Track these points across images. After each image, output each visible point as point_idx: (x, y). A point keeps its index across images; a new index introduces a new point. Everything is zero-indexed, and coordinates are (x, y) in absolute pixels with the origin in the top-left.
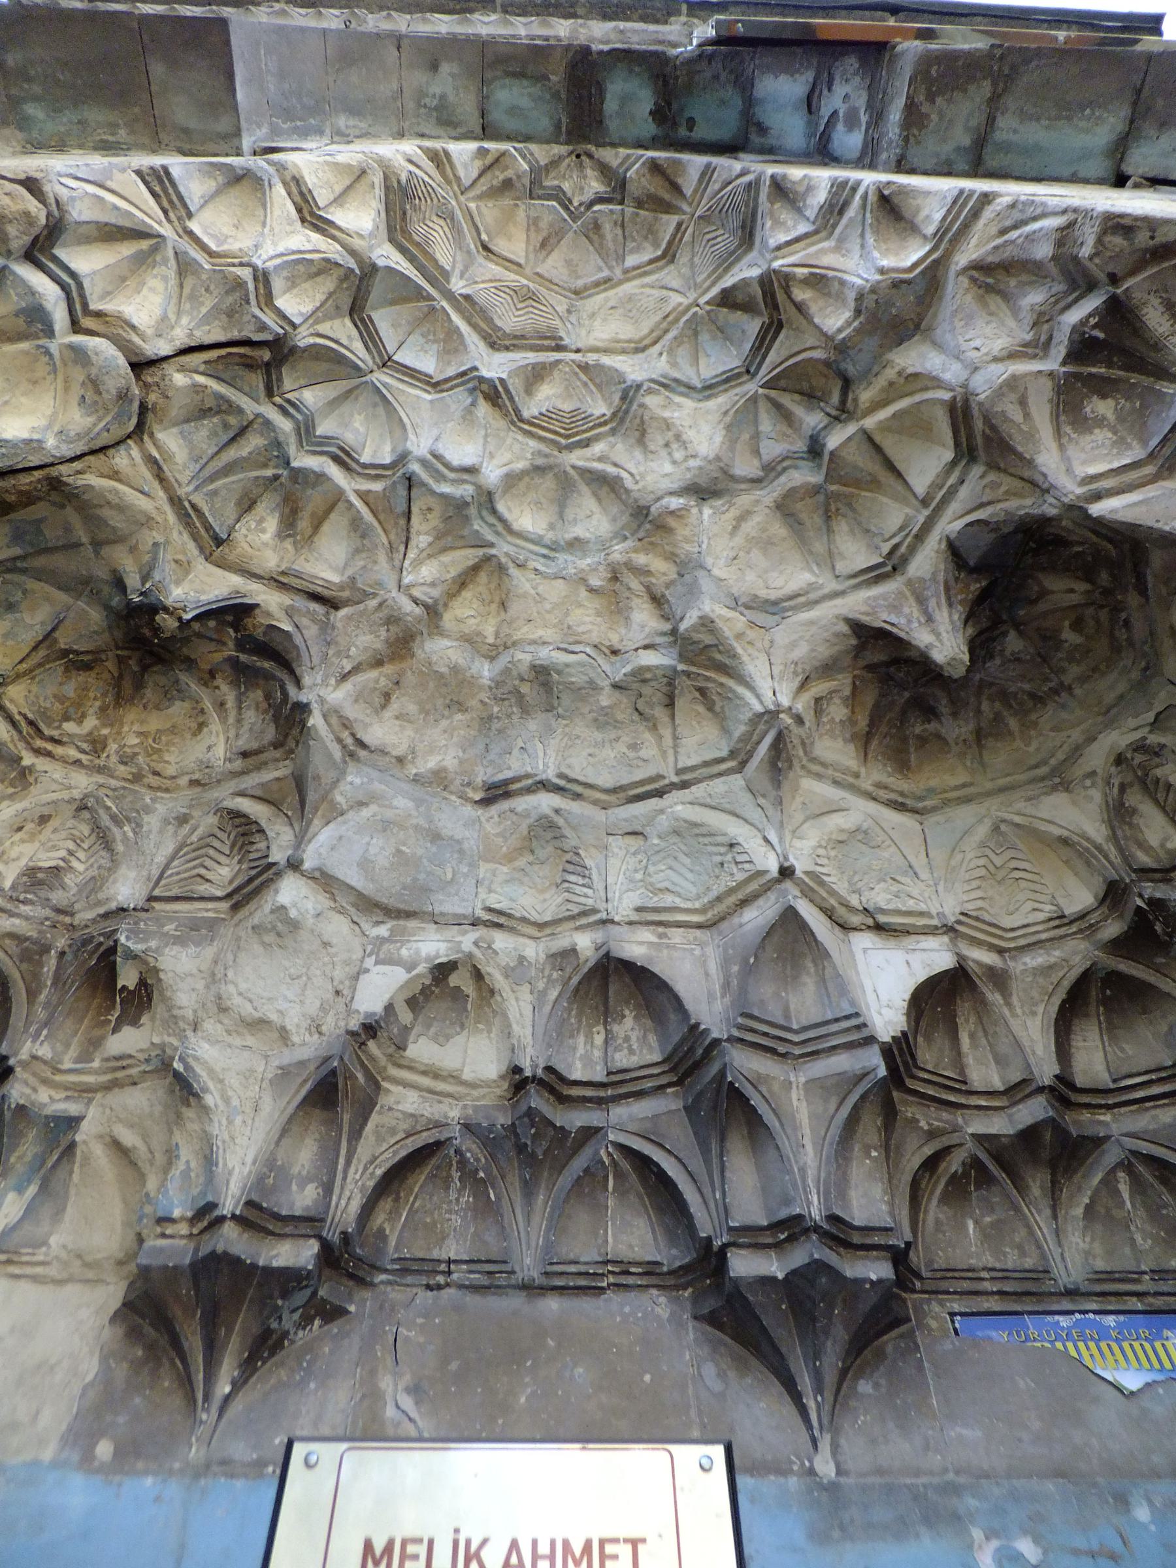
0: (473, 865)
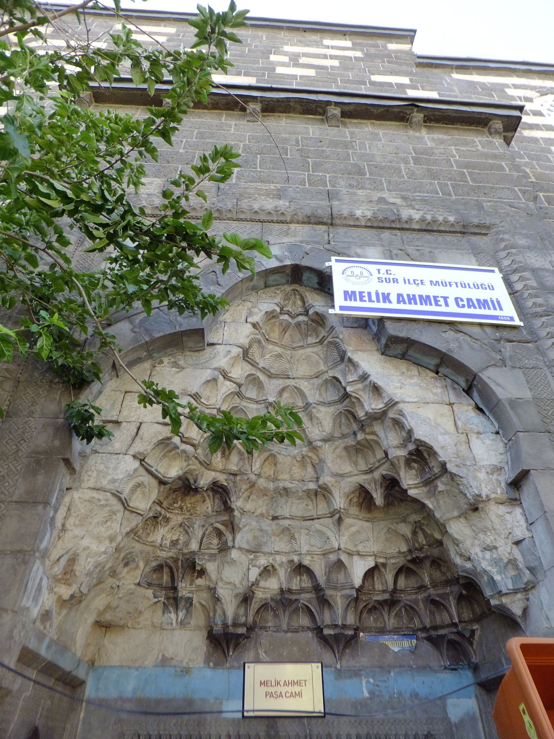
0: (270, 537)
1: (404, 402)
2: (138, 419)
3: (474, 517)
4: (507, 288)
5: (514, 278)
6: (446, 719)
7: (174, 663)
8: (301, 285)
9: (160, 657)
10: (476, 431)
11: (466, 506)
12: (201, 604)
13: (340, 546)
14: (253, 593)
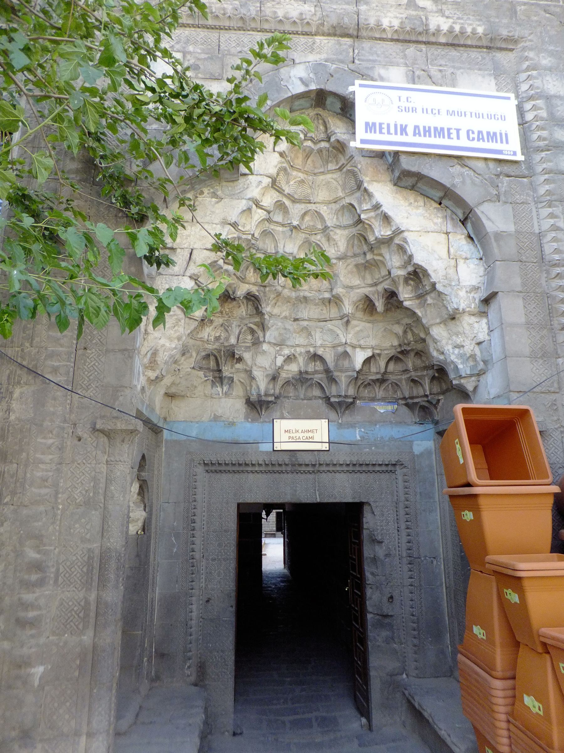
0: (292, 334)
1: (408, 231)
2: (190, 245)
3: (451, 324)
4: (518, 118)
5: (528, 106)
6: (411, 452)
7: (223, 419)
8: (324, 109)
9: (213, 415)
10: (464, 257)
11: (446, 316)
12: (240, 381)
13: (346, 341)
14: (279, 374)
